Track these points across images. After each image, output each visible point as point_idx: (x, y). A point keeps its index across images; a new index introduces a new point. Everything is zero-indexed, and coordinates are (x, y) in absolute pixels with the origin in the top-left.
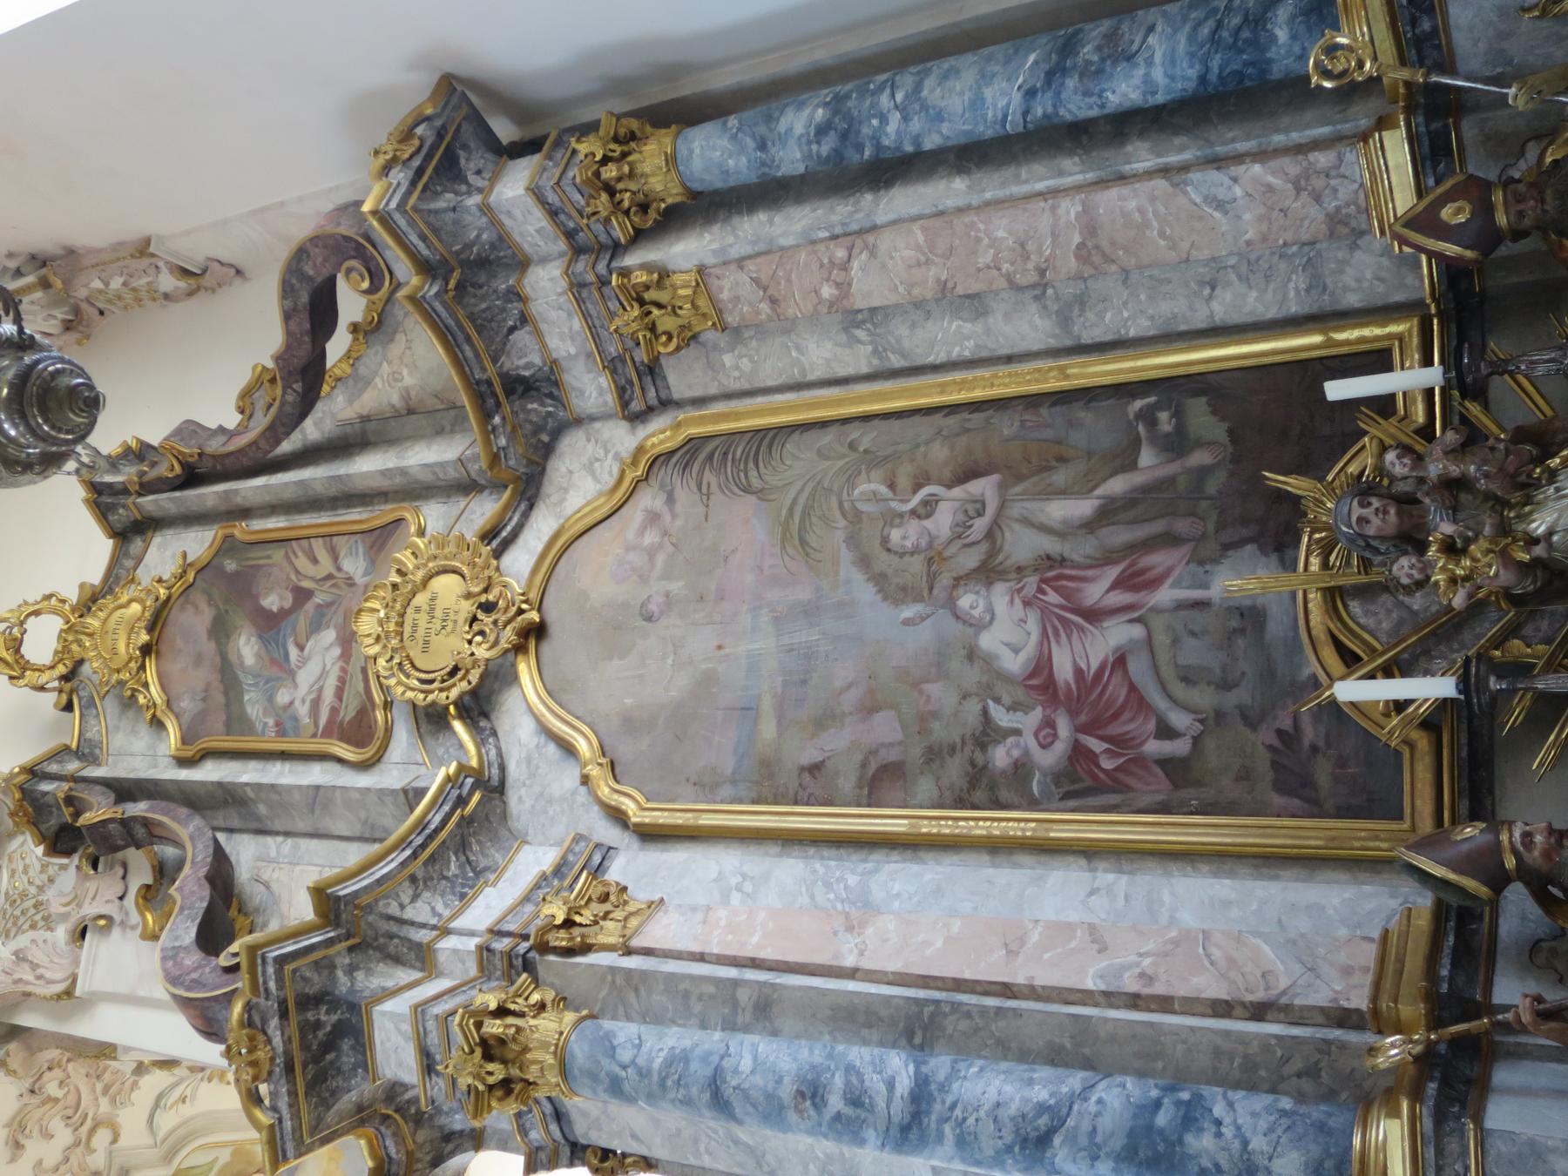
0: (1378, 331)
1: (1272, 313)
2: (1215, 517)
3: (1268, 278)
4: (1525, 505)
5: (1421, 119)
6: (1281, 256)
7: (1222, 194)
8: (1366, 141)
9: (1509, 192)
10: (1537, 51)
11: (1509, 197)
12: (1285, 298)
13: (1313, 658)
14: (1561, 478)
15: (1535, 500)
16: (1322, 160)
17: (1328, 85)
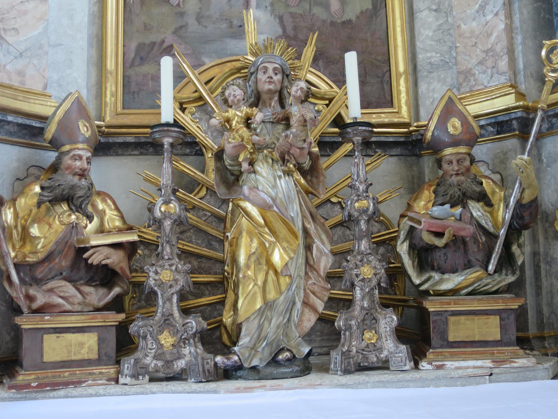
0: (403, 101)
1: (419, 45)
2: (299, 12)
3: (439, 41)
4: (273, 160)
5: (519, 114)
6: (451, 47)
7: (489, 7)
8: (511, 86)
9: (464, 156)
10: (553, 180)
11: (461, 156)
12: (427, 51)
13: (214, 64)
14: (287, 178)
15: (275, 165)
16: (503, 64)
17: (543, 53)
